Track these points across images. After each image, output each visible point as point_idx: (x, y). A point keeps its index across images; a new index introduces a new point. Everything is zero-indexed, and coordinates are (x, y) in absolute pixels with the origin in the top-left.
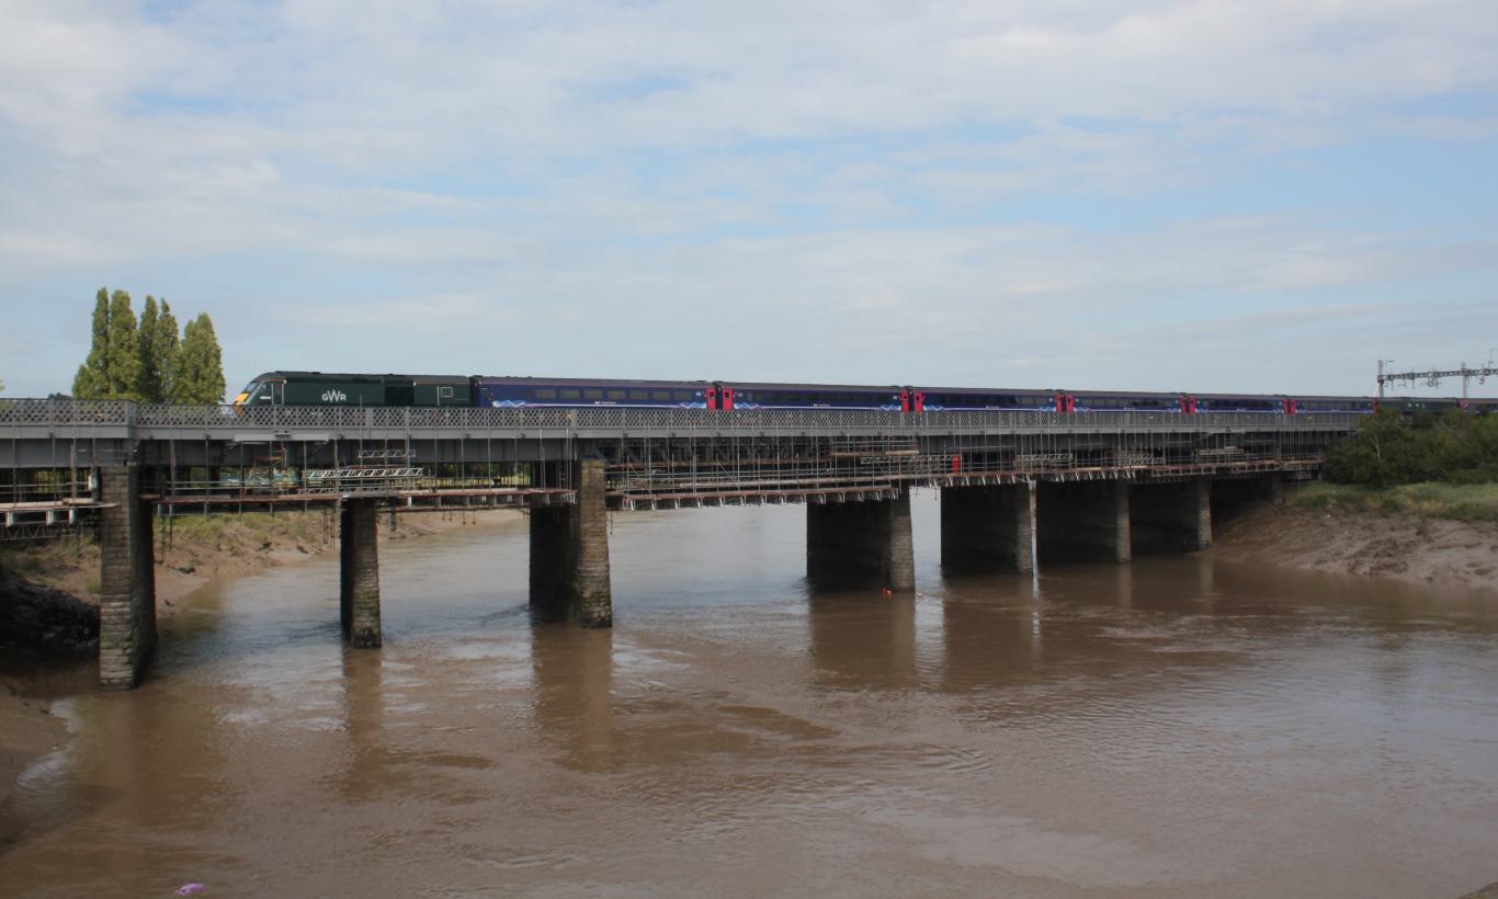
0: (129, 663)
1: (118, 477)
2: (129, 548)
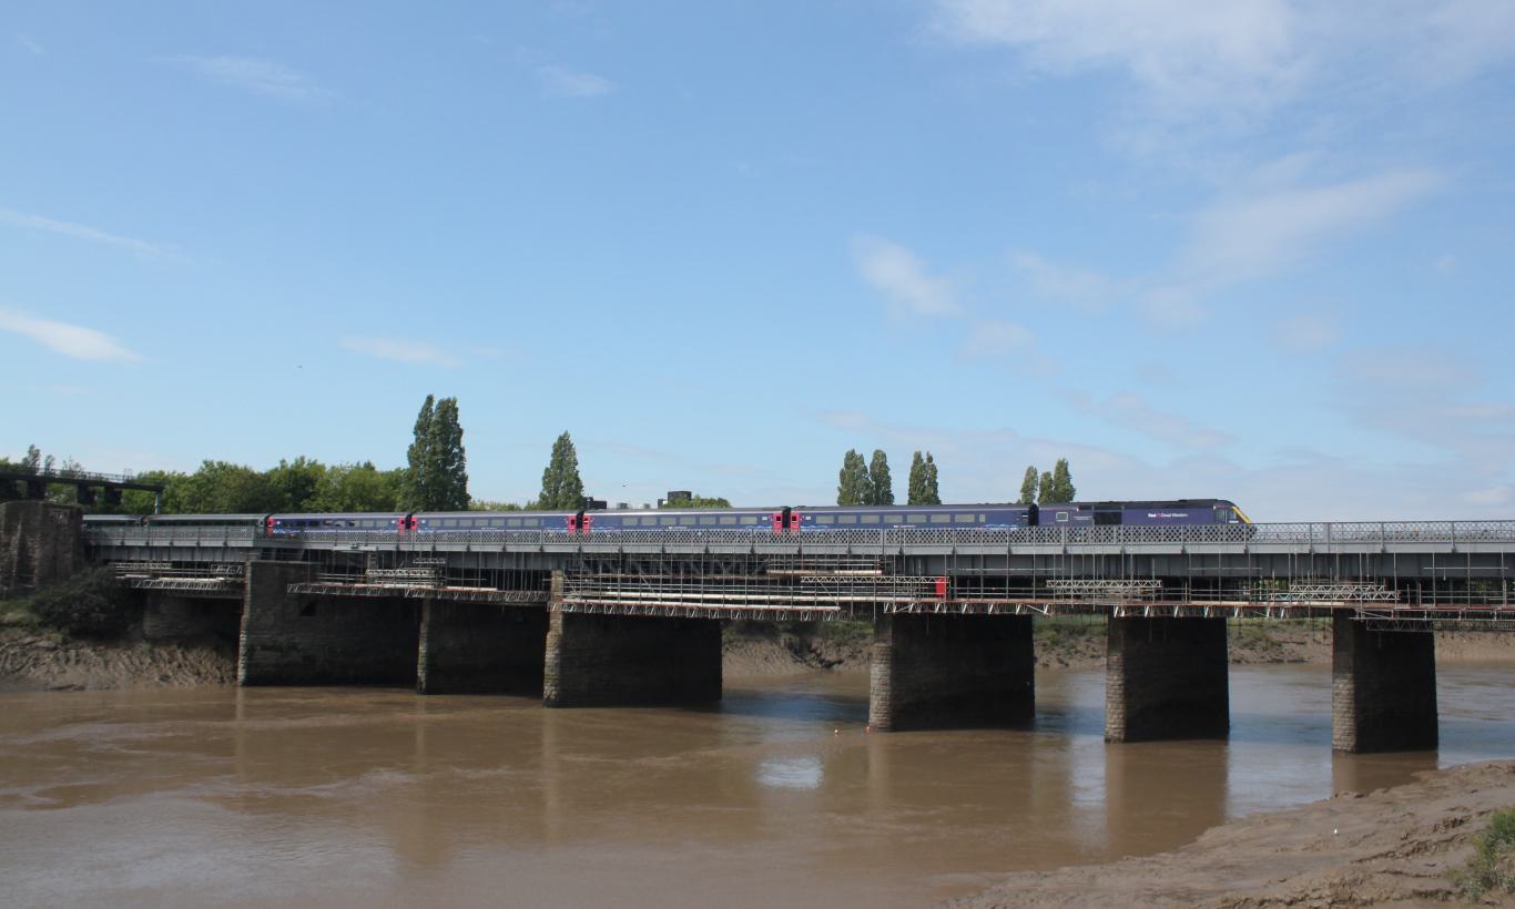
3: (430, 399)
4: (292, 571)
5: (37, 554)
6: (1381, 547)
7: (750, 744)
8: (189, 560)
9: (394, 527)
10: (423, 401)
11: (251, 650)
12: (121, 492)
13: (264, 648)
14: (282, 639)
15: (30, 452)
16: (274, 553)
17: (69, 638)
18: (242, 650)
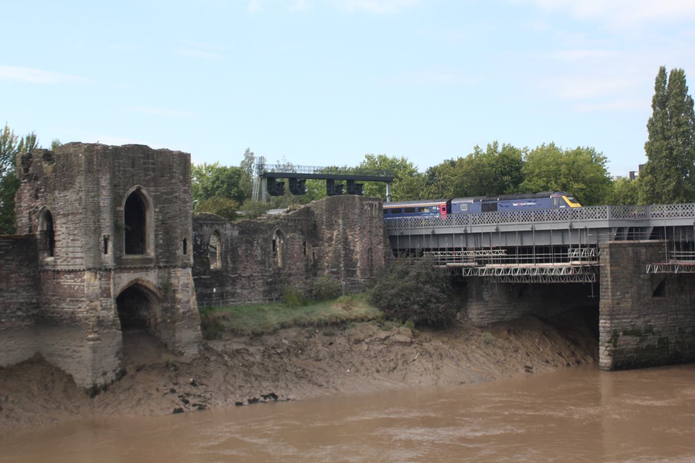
0: (609, 355)
1: (605, 250)
2: (610, 290)
3: (663, 71)
4: (643, 250)
5: (358, 248)
6: (431, 230)
7: (81, 346)
8: (560, 243)
9: (436, 212)
10: (656, 72)
11: (615, 336)
12: (362, 185)
13: (626, 333)
14: (640, 323)
15: (247, 157)
16: (626, 232)
17: (417, 331)
18: (604, 337)
